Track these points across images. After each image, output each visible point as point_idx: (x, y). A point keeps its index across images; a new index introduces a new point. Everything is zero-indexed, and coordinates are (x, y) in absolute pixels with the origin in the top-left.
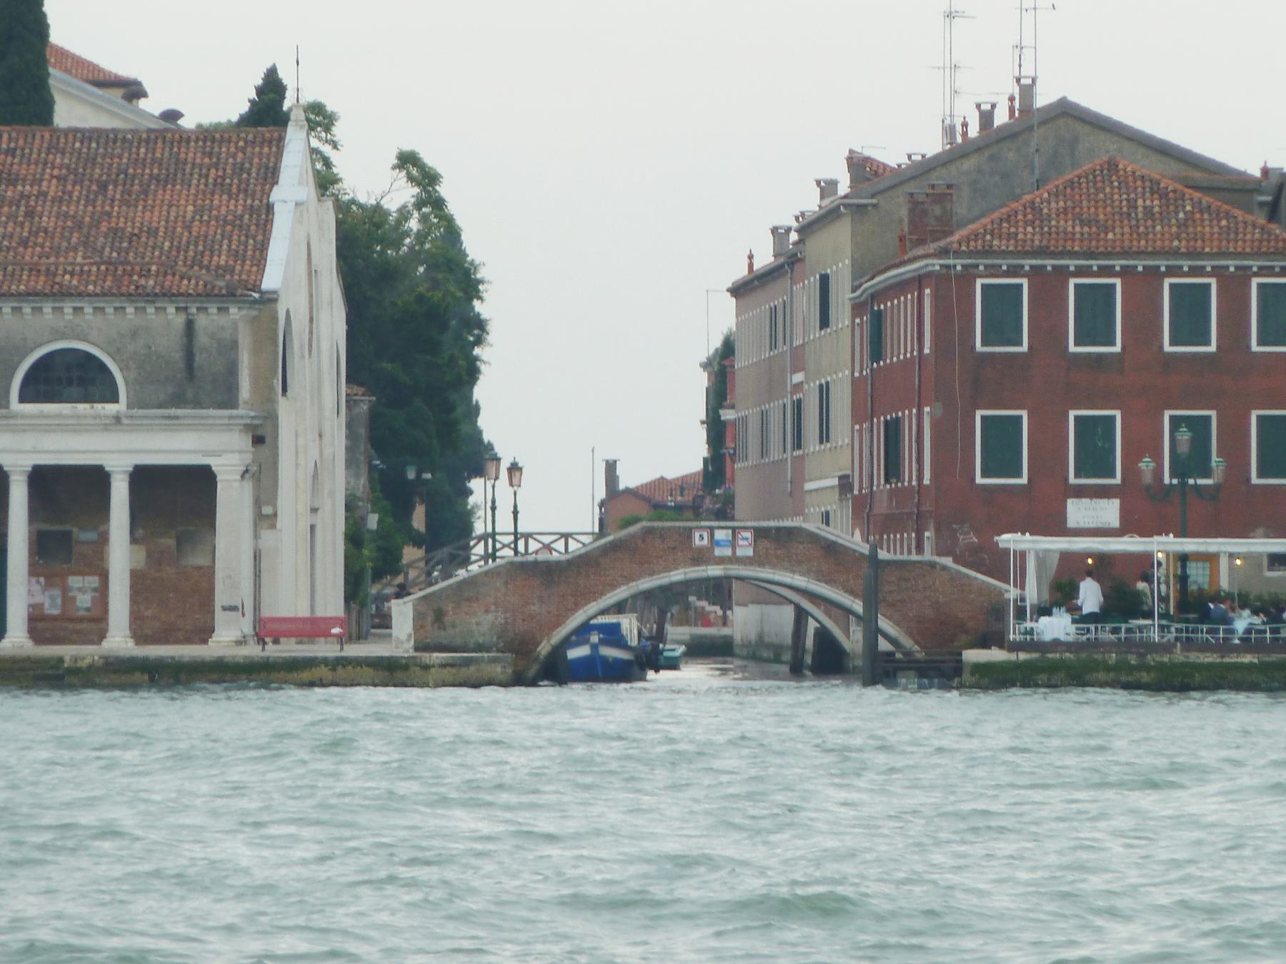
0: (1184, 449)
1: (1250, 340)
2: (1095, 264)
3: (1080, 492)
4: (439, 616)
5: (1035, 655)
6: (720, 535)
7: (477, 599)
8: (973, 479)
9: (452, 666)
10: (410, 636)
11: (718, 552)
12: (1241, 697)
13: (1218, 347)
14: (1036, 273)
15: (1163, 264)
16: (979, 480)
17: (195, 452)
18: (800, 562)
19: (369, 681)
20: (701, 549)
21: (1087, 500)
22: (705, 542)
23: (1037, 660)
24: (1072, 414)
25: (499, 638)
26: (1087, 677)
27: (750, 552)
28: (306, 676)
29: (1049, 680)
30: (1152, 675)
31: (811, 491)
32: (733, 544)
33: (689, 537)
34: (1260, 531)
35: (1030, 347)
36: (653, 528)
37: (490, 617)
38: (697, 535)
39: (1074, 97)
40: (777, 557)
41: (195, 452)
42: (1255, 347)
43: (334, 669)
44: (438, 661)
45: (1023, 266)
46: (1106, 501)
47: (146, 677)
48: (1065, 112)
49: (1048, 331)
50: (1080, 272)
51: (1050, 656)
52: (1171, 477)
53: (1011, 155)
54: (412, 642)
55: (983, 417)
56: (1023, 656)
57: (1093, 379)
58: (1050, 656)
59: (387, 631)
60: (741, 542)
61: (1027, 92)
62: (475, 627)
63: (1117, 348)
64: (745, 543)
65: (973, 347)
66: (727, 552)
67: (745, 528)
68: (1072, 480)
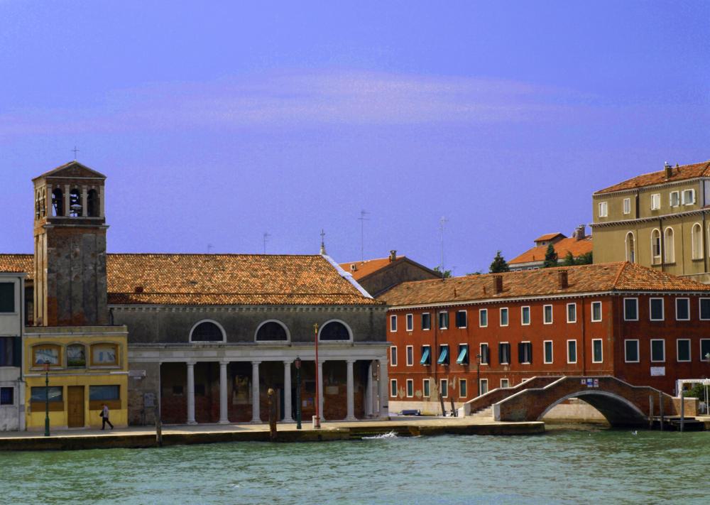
3: (655, 365)
11: (589, 386)
14: (666, 295)
15: (676, 293)
16: (626, 362)
17: (374, 355)
20: (584, 385)
27: (597, 386)
31: (384, 355)
32: (593, 383)
34: (703, 376)
37: (523, 409)
39: (408, 257)
41: (374, 355)
48: (405, 260)
53: (392, 272)
57: (658, 329)
59: (10, 362)
61: (394, 253)
63: (663, 319)
66: (591, 386)
67: (596, 378)
68: (652, 361)
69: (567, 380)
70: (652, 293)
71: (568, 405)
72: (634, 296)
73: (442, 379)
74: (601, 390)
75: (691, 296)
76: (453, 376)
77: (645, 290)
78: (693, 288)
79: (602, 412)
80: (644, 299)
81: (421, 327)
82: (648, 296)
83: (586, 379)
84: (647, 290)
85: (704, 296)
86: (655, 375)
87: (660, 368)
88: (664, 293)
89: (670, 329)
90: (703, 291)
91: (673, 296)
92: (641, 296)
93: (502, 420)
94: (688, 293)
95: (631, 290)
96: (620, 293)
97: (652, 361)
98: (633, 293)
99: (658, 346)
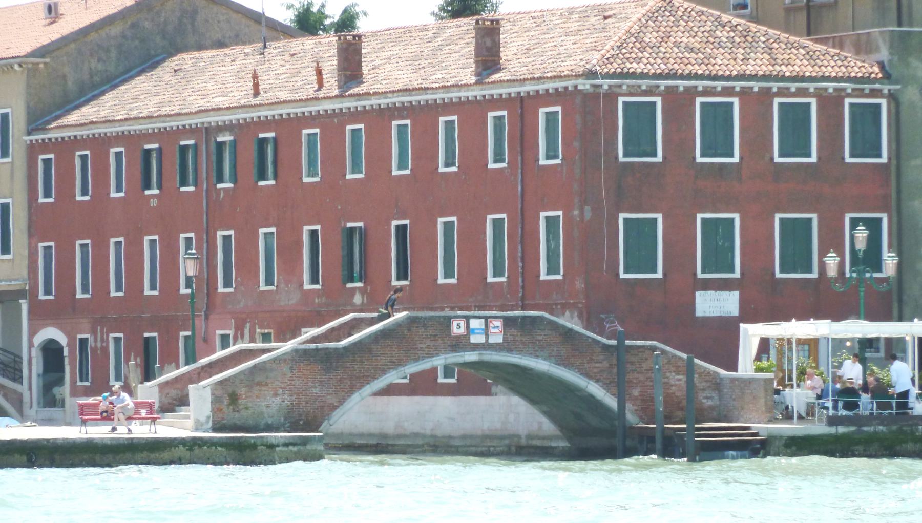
0: (861, 246)
1: (844, 153)
2: (719, 85)
3: (707, 285)
4: (234, 398)
5: (852, 429)
6: (475, 324)
7: (267, 384)
8: (618, 274)
9: (294, 444)
10: (208, 418)
11: (474, 339)
12: (449, 458)
13: (819, 158)
14: (744, 94)
15: (775, 86)
16: (622, 275)
18: (542, 348)
19: (223, 460)
20: (458, 337)
21: (713, 292)
22: (462, 330)
23: (853, 432)
24: (699, 216)
25: (285, 419)
26: (898, 448)
27: (499, 339)
28: (166, 455)
29: (865, 450)
30: (918, 445)
33: (449, 326)
35: (664, 158)
36: (417, 317)
37: (278, 400)
38: (455, 323)
40: (523, 343)
42: (848, 160)
43: (191, 450)
44: (282, 441)
45: (658, 86)
46: (727, 292)
47: (25, 458)
49: (679, 144)
50: (707, 92)
51: (865, 429)
52: (851, 271)
53: (147, 24)
54: (210, 424)
55: (625, 220)
56: (842, 430)
57: (717, 186)
58: (865, 429)
60: (493, 331)
62: (265, 409)
63: (736, 159)
64: (496, 330)
65: (617, 158)
68: (700, 275)
69: (412, 322)
70: (701, 85)
71: (488, 398)
72: (648, 92)
73: (219, 332)
74: (510, 350)
75: (820, 95)
76: (244, 322)
77: (682, 77)
78: (829, 71)
79: (547, 414)
80: (679, 104)
81: (255, 177)
82: (692, 93)
83: (467, 318)
84: (689, 77)
85: (859, 93)
86: (709, 313)
87: (725, 294)
88: (738, 85)
89: (761, 187)
90: (855, 80)
91: (767, 95)
92: (670, 95)
93: (215, 429)
94: (738, 85)
95: (643, 76)
96: (606, 84)
97: (700, 275)
98: (644, 84)
99: (718, 232)
